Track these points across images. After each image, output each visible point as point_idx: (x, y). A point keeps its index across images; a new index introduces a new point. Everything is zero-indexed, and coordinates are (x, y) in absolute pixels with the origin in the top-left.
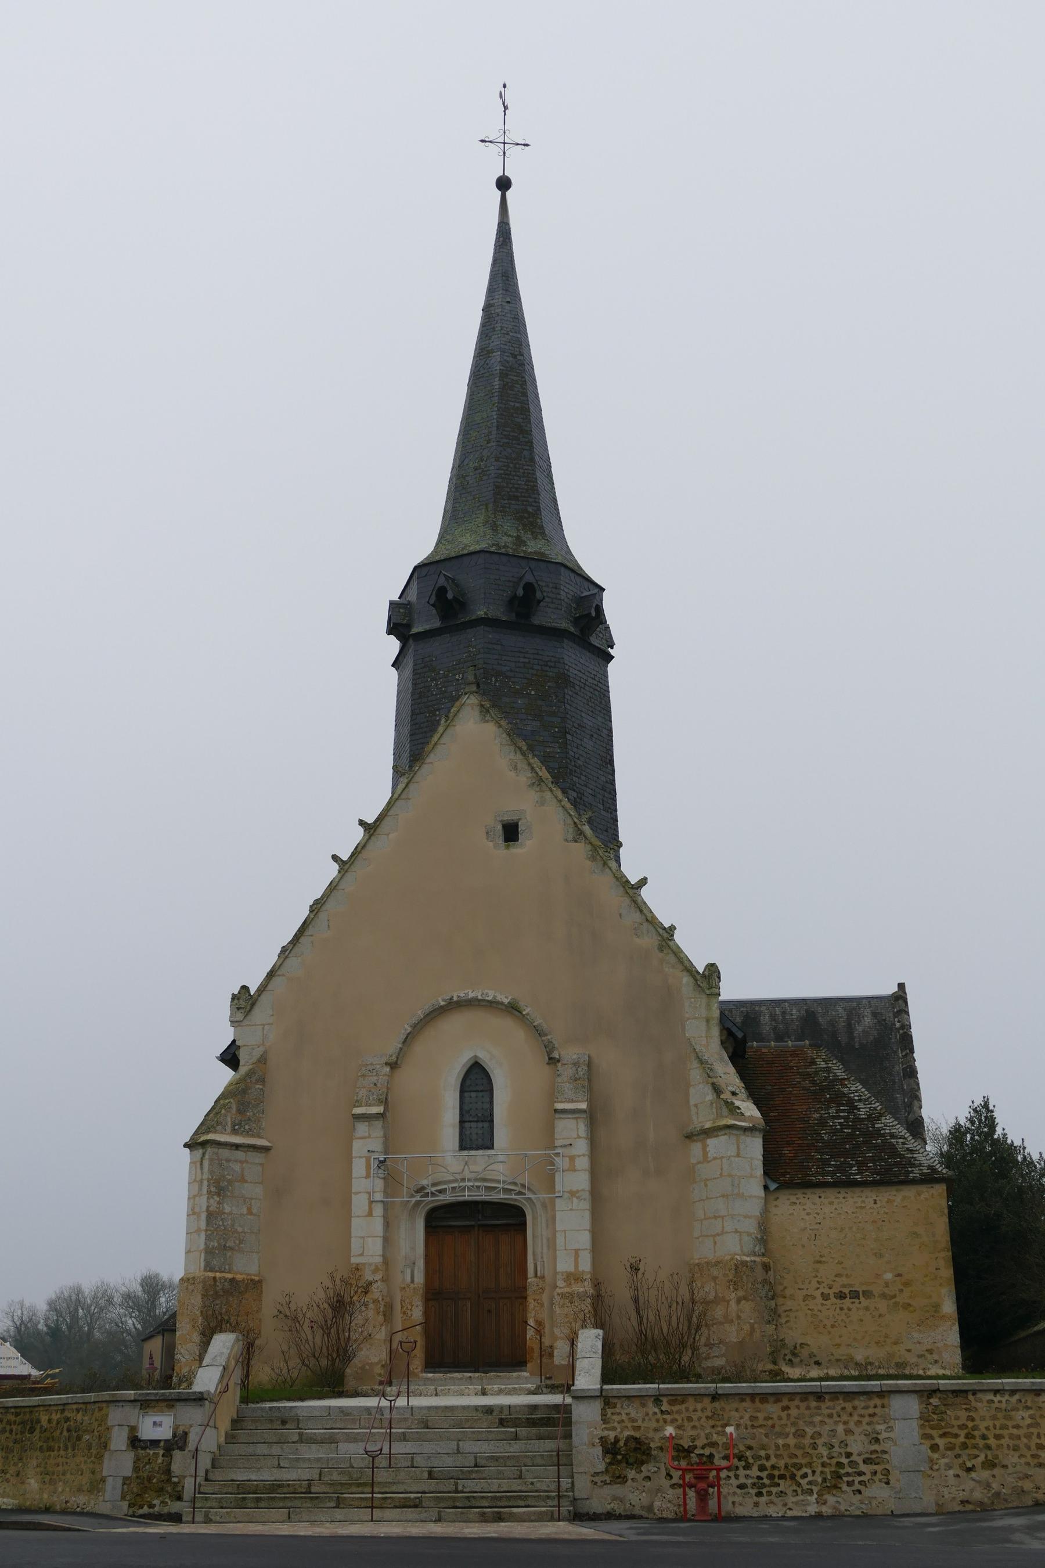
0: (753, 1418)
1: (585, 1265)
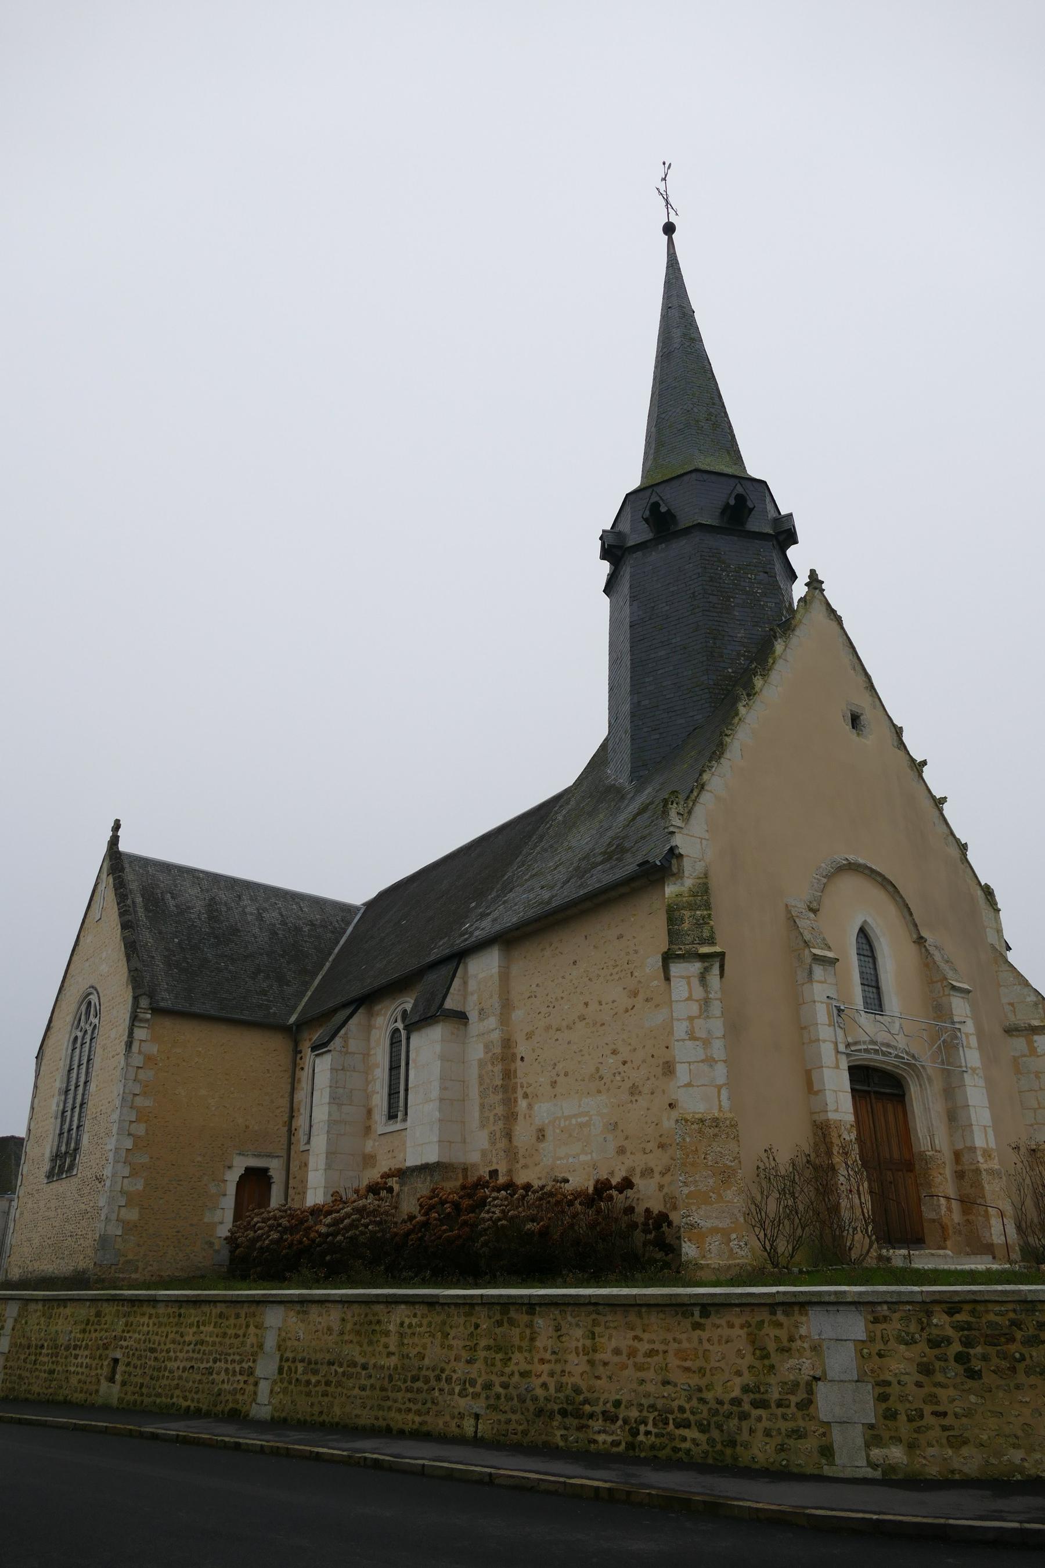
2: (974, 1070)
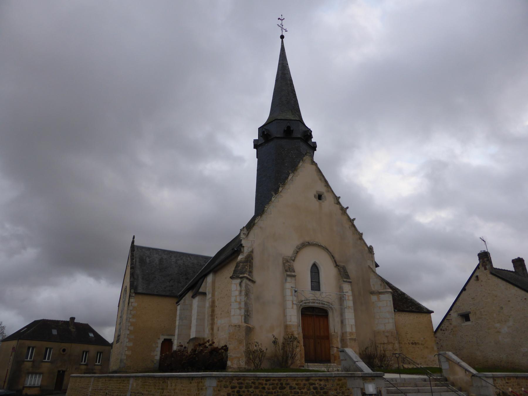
2: (349, 307)
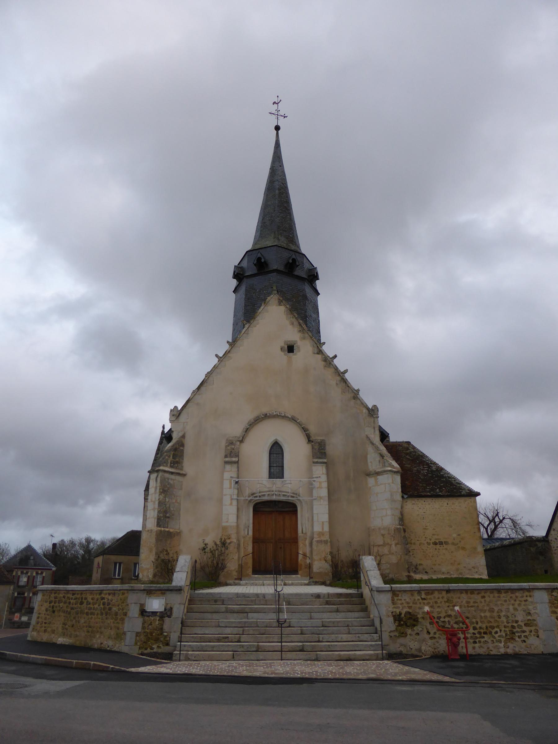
0: (468, 602)
1: (326, 528)
2: (321, 498)
